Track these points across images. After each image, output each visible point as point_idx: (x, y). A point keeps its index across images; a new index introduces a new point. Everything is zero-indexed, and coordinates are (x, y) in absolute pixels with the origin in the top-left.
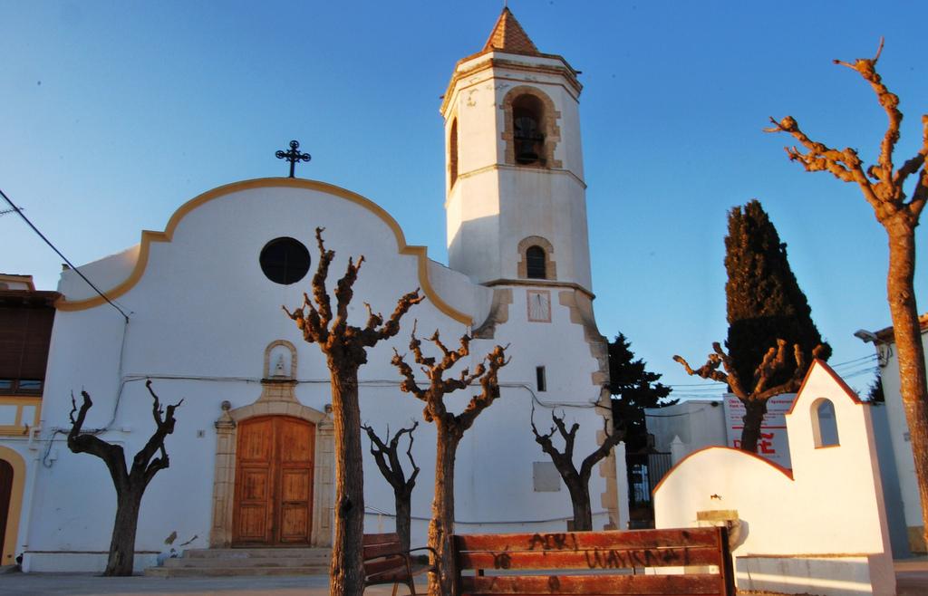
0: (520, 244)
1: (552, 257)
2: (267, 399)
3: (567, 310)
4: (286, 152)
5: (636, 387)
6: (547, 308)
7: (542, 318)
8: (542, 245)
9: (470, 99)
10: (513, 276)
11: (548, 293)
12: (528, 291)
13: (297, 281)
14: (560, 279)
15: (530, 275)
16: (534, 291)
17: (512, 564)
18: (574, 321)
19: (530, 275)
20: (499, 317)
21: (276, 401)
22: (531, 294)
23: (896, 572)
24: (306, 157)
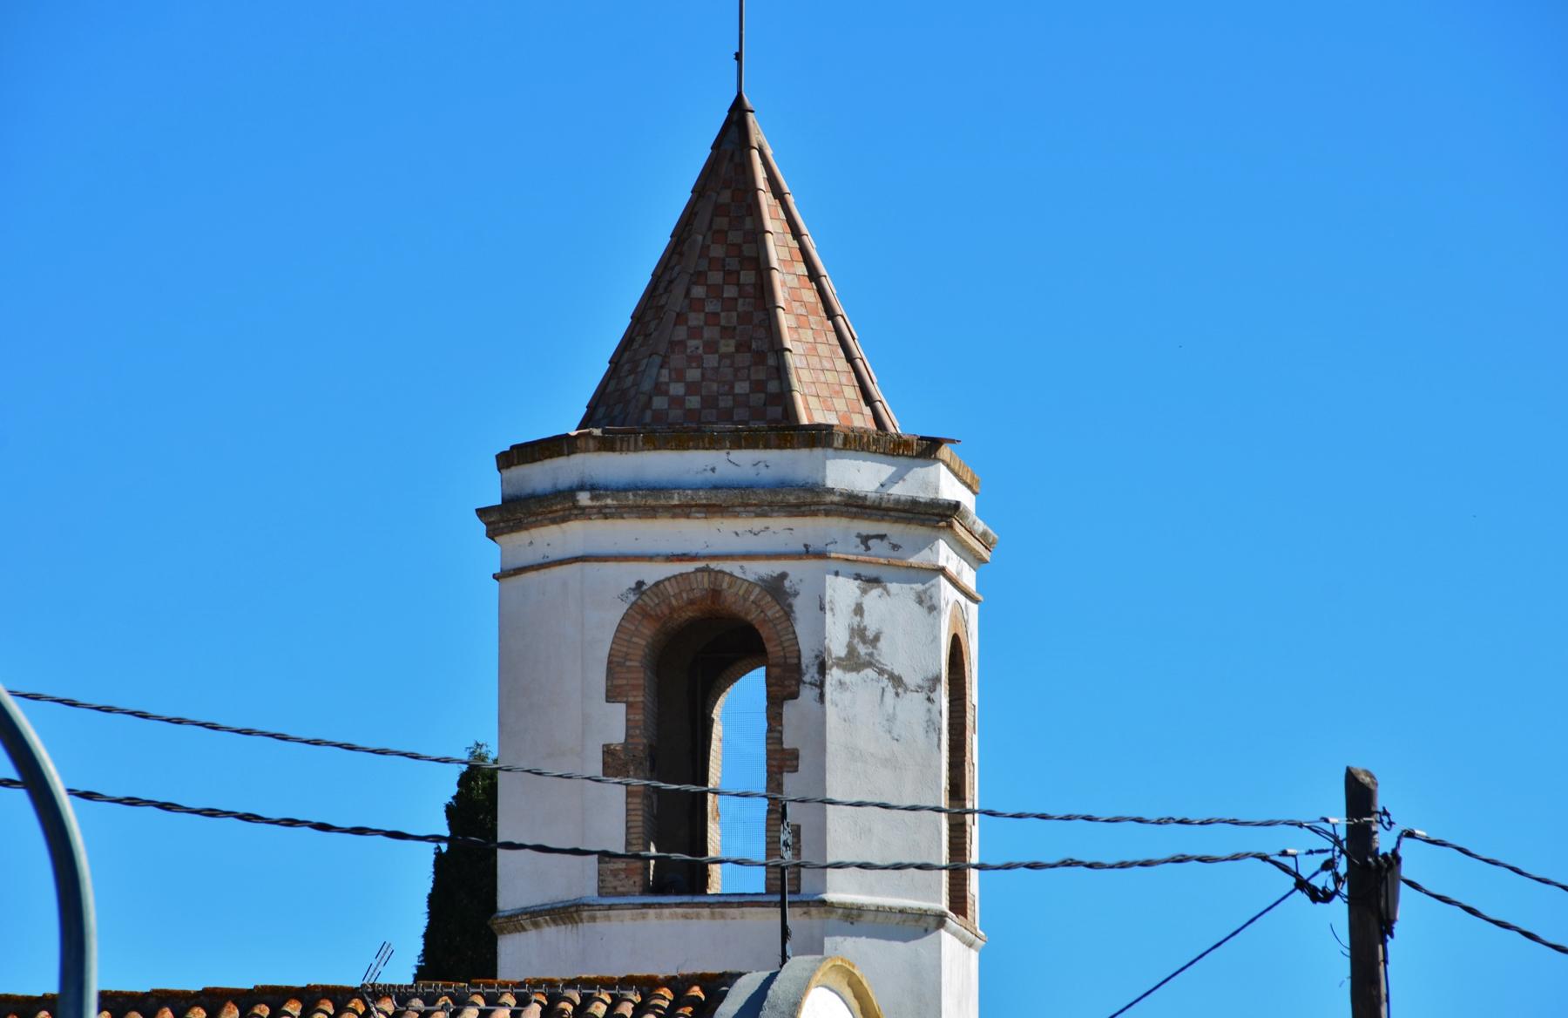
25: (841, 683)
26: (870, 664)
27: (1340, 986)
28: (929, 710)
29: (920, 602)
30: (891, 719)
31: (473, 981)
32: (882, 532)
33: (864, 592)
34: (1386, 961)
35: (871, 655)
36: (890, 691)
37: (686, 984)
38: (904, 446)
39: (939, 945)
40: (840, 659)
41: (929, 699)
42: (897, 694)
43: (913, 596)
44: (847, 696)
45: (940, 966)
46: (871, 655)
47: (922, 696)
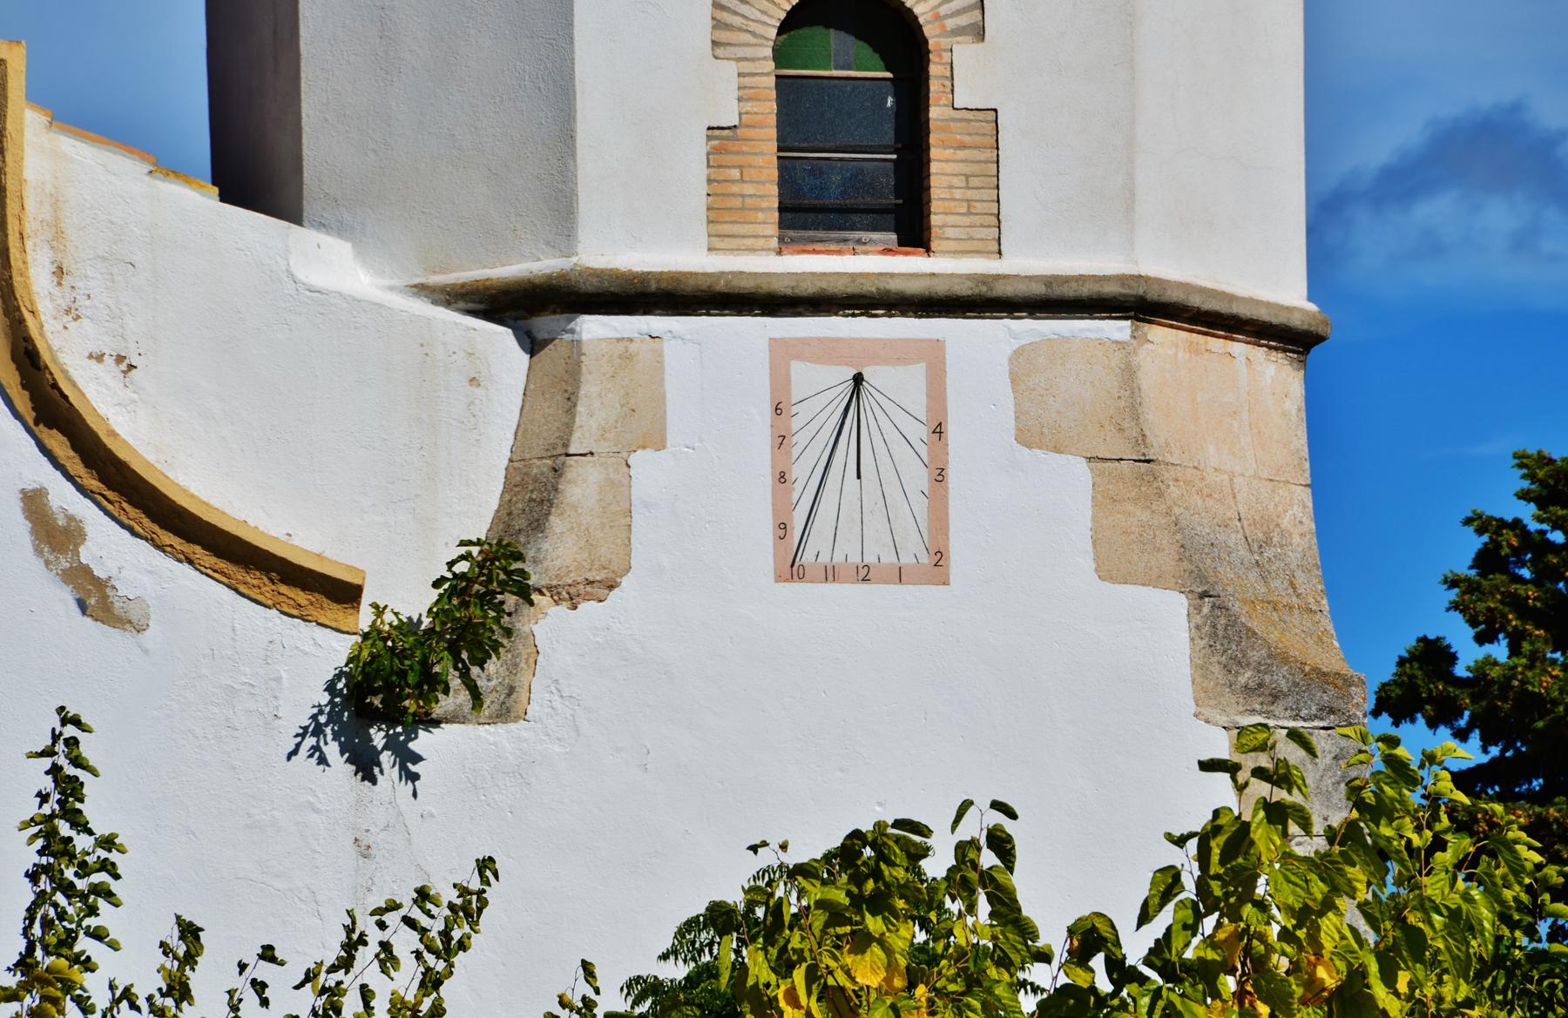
6: (918, 478)
7: (878, 551)
11: (934, 357)
12: (782, 353)
16: (827, 351)
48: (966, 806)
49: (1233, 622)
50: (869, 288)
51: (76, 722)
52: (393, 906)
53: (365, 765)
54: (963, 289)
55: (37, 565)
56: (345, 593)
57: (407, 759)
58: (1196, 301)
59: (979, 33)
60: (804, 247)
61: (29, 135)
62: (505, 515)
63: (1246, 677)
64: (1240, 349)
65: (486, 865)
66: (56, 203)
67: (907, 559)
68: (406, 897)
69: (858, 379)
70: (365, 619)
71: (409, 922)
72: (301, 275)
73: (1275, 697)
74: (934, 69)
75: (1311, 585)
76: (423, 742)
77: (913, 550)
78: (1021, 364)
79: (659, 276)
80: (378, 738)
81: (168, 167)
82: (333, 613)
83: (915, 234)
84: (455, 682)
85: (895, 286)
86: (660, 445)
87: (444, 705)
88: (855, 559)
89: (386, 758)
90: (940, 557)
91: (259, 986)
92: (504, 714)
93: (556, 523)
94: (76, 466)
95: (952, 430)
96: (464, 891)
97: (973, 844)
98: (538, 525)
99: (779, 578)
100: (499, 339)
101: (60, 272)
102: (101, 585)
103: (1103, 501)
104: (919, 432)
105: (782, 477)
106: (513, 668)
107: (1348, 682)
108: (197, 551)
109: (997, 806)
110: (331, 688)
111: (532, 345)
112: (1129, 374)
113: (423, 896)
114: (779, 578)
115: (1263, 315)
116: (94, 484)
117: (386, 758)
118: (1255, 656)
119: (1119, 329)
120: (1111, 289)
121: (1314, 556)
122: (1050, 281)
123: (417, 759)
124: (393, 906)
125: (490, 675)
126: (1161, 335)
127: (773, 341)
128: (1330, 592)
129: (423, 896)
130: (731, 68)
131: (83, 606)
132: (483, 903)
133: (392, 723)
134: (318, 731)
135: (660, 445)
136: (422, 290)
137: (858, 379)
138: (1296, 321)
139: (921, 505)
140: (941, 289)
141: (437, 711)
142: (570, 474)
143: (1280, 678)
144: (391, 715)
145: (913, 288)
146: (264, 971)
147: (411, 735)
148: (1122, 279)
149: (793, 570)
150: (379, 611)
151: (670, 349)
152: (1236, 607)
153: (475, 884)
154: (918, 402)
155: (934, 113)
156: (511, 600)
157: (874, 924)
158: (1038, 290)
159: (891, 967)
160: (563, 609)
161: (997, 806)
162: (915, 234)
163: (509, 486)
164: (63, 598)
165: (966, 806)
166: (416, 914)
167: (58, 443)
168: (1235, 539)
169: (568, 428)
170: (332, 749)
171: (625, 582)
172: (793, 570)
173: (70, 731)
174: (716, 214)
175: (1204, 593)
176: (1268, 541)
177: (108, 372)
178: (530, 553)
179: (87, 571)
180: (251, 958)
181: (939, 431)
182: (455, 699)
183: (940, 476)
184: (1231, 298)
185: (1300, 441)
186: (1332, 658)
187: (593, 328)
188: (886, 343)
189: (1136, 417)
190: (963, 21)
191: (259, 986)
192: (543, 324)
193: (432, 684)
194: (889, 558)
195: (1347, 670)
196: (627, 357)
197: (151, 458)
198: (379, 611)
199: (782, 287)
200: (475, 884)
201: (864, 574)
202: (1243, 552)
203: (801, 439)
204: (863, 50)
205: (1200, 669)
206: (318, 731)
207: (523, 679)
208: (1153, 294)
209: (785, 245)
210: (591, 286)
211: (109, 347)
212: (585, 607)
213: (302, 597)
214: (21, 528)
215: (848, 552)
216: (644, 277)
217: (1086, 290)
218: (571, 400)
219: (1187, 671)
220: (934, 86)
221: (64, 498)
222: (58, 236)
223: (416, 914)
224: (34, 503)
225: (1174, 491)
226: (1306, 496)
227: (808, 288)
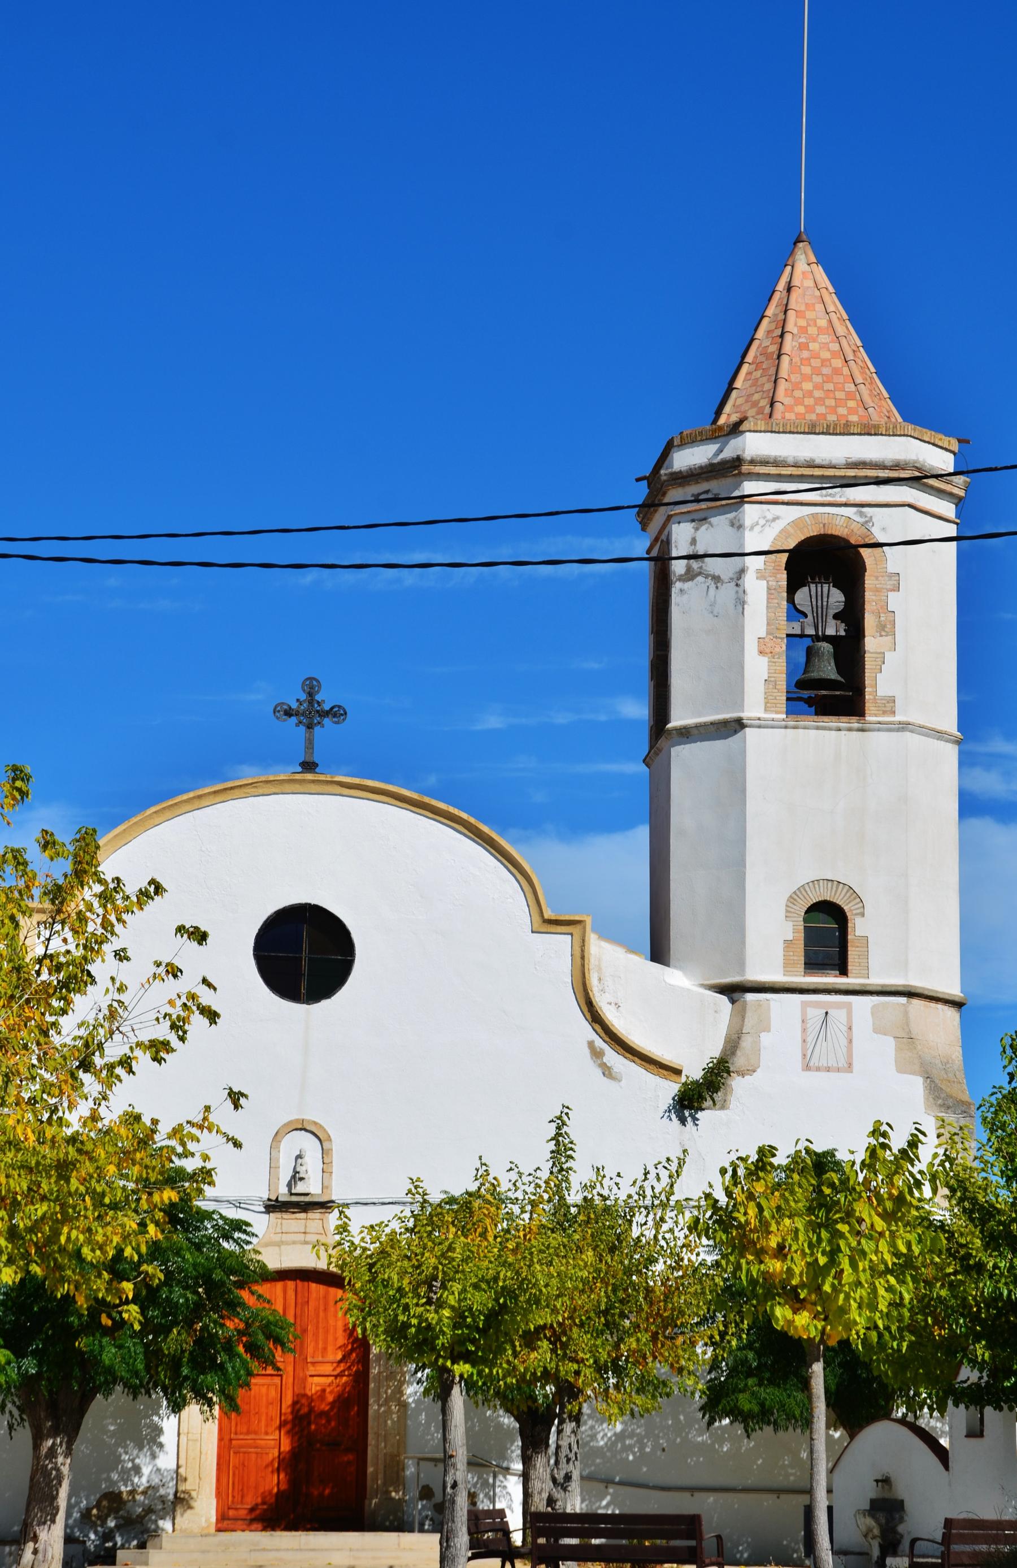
0: (792, 899)
1: (858, 928)
2: (277, 1238)
3: (888, 1044)
4: (294, 705)
5: (760, 1462)
6: (844, 1042)
7: (832, 1063)
8: (839, 898)
9: (694, 542)
10: (777, 977)
11: (849, 1006)
12: (805, 1005)
13: (329, 997)
14: (876, 979)
15: (812, 965)
16: (817, 1005)
17: (411, 1519)
18: (902, 1068)
19: (812, 965)
20: (738, 1062)
21: (294, 1243)
22: (811, 1012)
23: (225, 1522)
24: (337, 713)
25: (681, 590)
26: (700, 574)
27: (237, 1144)
28: (737, 592)
29: (732, 525)
30: (713, 604)
31: (3, 1193)
32: (707, 488)
33: (697, 529)
34: (818, 728)
35: (701, 568)
36: (713, 586)
37: (46, 1116)
38: (708, 1089)
39: (744, 740)
40: (681, 575)
41: (737, 585)
42: (717, 588)
43: (727, 523)
44: (686, 597)
45: (745, 751)
46: (701, 568)
47: (733, 584)
48: (798, 1140)
49: (936, 1086)
50: (830, 987)
51: (568, 1108)
52: (660, 1163)
53: (683, 1121)
54: (857, 988)
55: (592, 1062)
56: (678, 1072)
57: (695, 1119)
58: (926, 993)
59: (863, 915)
60: (811, 975)
61: (592, 941)
62: (724, 1050)
63: (940, 1102)
64: (940, 1006)
65: (685, 1151)
66: (599, 960)
67: (840, 1065)
68: (664, 1160)
69: (827, 1013)
70: (683, 1079)
71: (665, 1168)
72: (667, 981)
73: (948, 1108)
74: (849, 925)
75: (961, 1076)
76: (700, 1115)
77: (842, 1063)
78: (875, 1010)
79: (769, 983)
80: (687, 1113)
81: (632, 950)
82: (674, 1077)
83: (844, 972)
84: (708, 1099)
85: (837, 987)
86: (769, 1031)
87: (705, 1104)
88: (825, 1065)
89: (689, 1119)
90: (850, 1065)
91: (617, 1184)
92: (723, 1107)
93: (739, 1053)
94: (603, 1034)
95: (854, 1028)
96: (679, 1159)
97: (800, 1151)
98: (733, 1053)
99: (803, 1070)
100: (724, 999)
101: (600, 979)
102: (609, 1068)
103: (898, 1049)
104: (844, 1029)
105: (804, 1041)
106: (726, 1094)
107: (970, 1104)
108: (636, 1059)
109: (807, 1140)
110: (673, 1099)
111: (733, 1002)
112: (906, 1013)
113: (668, 1160)
114: (803, 1070)
115: (947, 997)
116: (608, 1039)
117: (689, 1119)
118: (943, 1096)
119: (903, 1000)
120: (900, 989)
121: (962, 1067)
122: (883, 986)
123: (698, 1120)
124: (660, 1163)
125: (719, 1096)
126: (916, 1002)
127: (802, 1002)
128: (966, 1078)
129: (668, 1160)
130: (791, 924)
131: (604, 1074)
132: (684, 1163)
133: (691, 1109)
134: (670, 1111)
135: (769, 1031)
136: (703, 986)
137: (827, 1013)
138: (957, 999)
139: (845, 1050)
140: (851, 988)
141: (704, 1106)
142: (743, 1039)
143: (950, 1102)
144: (690, 1107)
145: (843, 987)
146: (618, 1180)
147: (696, 1113)
148: (904, 986)
149: (807, 1067)
150: (688, 1077)
151: (772, 1003)
152: (937, 1081)
153: (682, 1157)
154: (844, 1020)
155: (849, 937)
156: (725, 1075)
157: (761, 1174)
158: (879, 989)
159: (767, 1186)
160: (740, 1078)
161: (807, 1140)
162: (844, 972)
163: (726, 1042)
164: (599, 1072)
165: (798, 1140)
166: (666, 1165)
167: (597, 1027)
168: (937, 1061)
169: (742, 1026)
170: (673, 1116)
171: (758, 1070)
172: (807, 1067)
173: (566, 1110)
174: (786, 965)
175: (928, 1077)
176: (948, 1062)
177: (613, 1008)
178: (731, 1061)
179: (605, 1064)
180: (614, 1176)
181: (850, 1028)
182: (708, 1103)
183: (850, 1041)
184: (937, 992)
185: (958, 1033)
186: (966, 1097)
187: (750, 997)
188: (811, 1002)
189: (908, 1025)
190: (858, 911)
191: (617, 1184)
192: (736, 995)
193: (701, 1098)
194: (835, 1065)
195: (970, 1100)
196: (760, 1005)
197: (624, 1032)
198: (688, 1077)
199: (805, 987)
200: (682, 1157)
201: (828, 1070)
202: (940, 1065)
203: (809, 1030)
204: (830, 919)
205: (926, 1099)
206: (670, 1111)
207: (728, 1097)
208: (913, 991)
209: (806, 974)
210: (749, 985)
211: (613, 1000)
212: (746, 1077)
213: (665, 1073)
214: (587, 1051)
215: (823, 1063)
216: (764, 983)
217: (893, 989)
218: (743, 1018)
219: (922, 1100)
220: (849, 930)
221: (599, 1043)
222: (599, 969)
223: (666, 1165)
224: (591, 1044)
225: (919, 1047)
226: (960, 1049)
227: (812, 987)
